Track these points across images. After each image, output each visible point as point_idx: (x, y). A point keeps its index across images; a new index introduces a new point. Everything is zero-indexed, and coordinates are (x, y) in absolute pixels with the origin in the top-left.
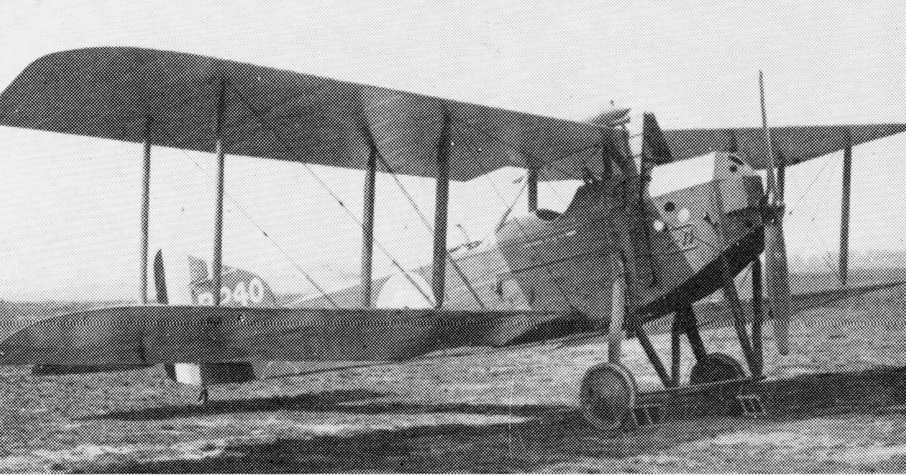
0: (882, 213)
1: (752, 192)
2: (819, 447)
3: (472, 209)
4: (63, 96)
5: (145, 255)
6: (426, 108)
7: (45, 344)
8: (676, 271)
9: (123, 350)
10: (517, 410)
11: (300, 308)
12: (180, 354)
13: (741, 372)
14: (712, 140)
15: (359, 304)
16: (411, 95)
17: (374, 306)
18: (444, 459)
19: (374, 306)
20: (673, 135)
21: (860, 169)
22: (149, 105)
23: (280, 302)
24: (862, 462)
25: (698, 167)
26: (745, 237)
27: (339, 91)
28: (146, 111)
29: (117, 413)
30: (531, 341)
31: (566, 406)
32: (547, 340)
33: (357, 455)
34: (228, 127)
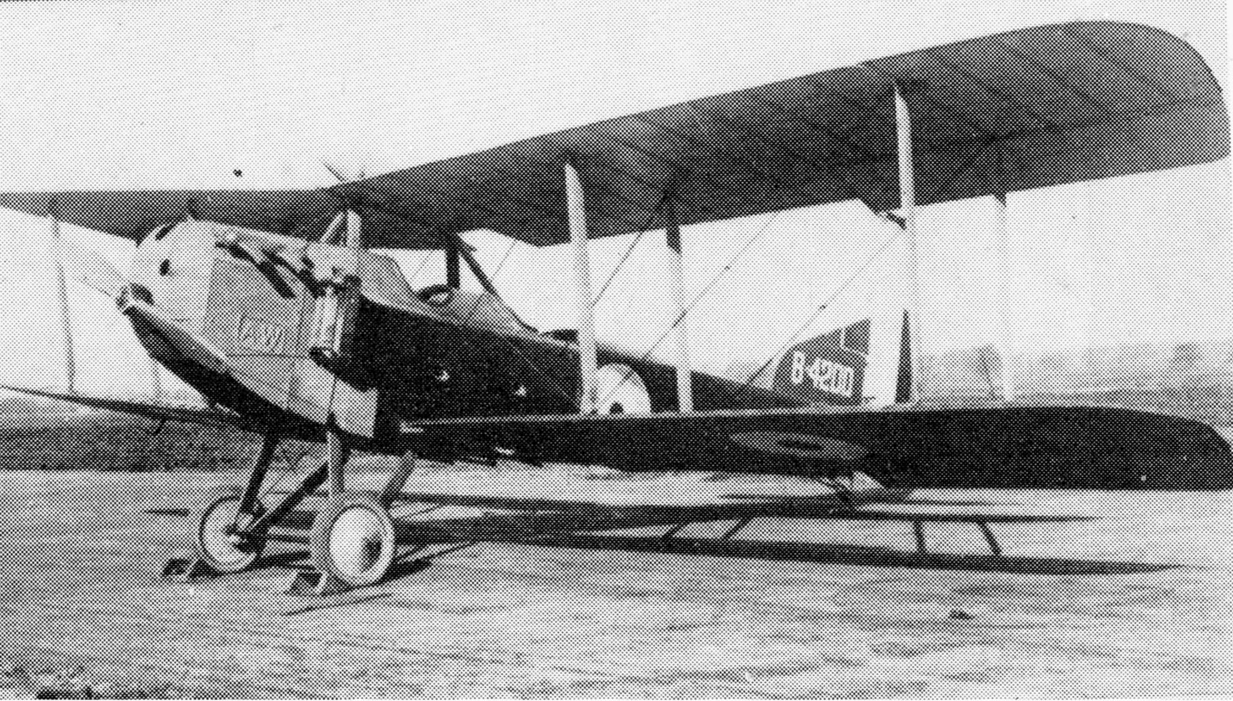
0: (1207, 308)
1: (155, 219)
2: (200, 615)
3: (1038, 324)
4: (128, 213)
5: (804, 697)
6: (115, 213)
7: (1161, 99)
8: (140, 212)
9: (983, 100)
10: (247, 211)
11: (274, 471)
12: (1048, 67)
13: (445, 303)
14: (94, 213)
15: (805, 635)
16: (17, 208)
17: (986, 681)
18: (1043, 107)
19: (986, 681)
20: (42, 208)
21: (701, 260)
22: (145, 217)
23: (237, 288)
24: (96, 655)
25: (939, 282)
26: (334, 237)
27: (100, 215)
28: (72, 209)
29: (276, 219)
30: (688, 469)
31: (215, 222)
32: (916, 552)
33: (495, 192)
34: (168, 218)
